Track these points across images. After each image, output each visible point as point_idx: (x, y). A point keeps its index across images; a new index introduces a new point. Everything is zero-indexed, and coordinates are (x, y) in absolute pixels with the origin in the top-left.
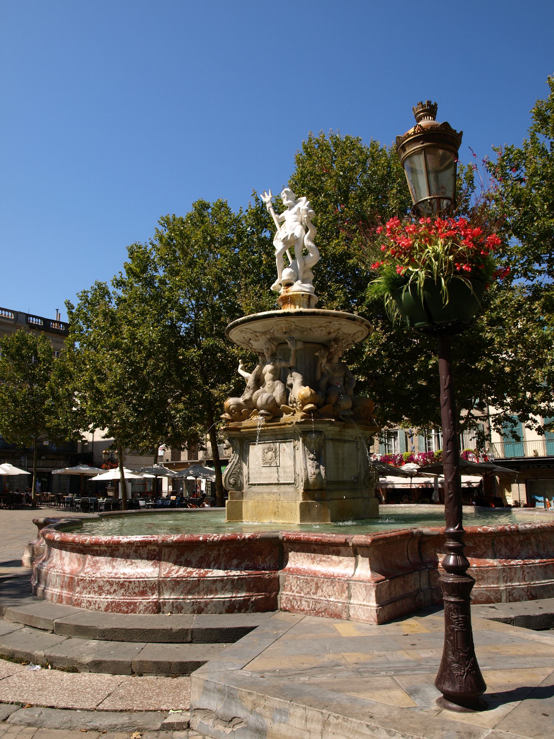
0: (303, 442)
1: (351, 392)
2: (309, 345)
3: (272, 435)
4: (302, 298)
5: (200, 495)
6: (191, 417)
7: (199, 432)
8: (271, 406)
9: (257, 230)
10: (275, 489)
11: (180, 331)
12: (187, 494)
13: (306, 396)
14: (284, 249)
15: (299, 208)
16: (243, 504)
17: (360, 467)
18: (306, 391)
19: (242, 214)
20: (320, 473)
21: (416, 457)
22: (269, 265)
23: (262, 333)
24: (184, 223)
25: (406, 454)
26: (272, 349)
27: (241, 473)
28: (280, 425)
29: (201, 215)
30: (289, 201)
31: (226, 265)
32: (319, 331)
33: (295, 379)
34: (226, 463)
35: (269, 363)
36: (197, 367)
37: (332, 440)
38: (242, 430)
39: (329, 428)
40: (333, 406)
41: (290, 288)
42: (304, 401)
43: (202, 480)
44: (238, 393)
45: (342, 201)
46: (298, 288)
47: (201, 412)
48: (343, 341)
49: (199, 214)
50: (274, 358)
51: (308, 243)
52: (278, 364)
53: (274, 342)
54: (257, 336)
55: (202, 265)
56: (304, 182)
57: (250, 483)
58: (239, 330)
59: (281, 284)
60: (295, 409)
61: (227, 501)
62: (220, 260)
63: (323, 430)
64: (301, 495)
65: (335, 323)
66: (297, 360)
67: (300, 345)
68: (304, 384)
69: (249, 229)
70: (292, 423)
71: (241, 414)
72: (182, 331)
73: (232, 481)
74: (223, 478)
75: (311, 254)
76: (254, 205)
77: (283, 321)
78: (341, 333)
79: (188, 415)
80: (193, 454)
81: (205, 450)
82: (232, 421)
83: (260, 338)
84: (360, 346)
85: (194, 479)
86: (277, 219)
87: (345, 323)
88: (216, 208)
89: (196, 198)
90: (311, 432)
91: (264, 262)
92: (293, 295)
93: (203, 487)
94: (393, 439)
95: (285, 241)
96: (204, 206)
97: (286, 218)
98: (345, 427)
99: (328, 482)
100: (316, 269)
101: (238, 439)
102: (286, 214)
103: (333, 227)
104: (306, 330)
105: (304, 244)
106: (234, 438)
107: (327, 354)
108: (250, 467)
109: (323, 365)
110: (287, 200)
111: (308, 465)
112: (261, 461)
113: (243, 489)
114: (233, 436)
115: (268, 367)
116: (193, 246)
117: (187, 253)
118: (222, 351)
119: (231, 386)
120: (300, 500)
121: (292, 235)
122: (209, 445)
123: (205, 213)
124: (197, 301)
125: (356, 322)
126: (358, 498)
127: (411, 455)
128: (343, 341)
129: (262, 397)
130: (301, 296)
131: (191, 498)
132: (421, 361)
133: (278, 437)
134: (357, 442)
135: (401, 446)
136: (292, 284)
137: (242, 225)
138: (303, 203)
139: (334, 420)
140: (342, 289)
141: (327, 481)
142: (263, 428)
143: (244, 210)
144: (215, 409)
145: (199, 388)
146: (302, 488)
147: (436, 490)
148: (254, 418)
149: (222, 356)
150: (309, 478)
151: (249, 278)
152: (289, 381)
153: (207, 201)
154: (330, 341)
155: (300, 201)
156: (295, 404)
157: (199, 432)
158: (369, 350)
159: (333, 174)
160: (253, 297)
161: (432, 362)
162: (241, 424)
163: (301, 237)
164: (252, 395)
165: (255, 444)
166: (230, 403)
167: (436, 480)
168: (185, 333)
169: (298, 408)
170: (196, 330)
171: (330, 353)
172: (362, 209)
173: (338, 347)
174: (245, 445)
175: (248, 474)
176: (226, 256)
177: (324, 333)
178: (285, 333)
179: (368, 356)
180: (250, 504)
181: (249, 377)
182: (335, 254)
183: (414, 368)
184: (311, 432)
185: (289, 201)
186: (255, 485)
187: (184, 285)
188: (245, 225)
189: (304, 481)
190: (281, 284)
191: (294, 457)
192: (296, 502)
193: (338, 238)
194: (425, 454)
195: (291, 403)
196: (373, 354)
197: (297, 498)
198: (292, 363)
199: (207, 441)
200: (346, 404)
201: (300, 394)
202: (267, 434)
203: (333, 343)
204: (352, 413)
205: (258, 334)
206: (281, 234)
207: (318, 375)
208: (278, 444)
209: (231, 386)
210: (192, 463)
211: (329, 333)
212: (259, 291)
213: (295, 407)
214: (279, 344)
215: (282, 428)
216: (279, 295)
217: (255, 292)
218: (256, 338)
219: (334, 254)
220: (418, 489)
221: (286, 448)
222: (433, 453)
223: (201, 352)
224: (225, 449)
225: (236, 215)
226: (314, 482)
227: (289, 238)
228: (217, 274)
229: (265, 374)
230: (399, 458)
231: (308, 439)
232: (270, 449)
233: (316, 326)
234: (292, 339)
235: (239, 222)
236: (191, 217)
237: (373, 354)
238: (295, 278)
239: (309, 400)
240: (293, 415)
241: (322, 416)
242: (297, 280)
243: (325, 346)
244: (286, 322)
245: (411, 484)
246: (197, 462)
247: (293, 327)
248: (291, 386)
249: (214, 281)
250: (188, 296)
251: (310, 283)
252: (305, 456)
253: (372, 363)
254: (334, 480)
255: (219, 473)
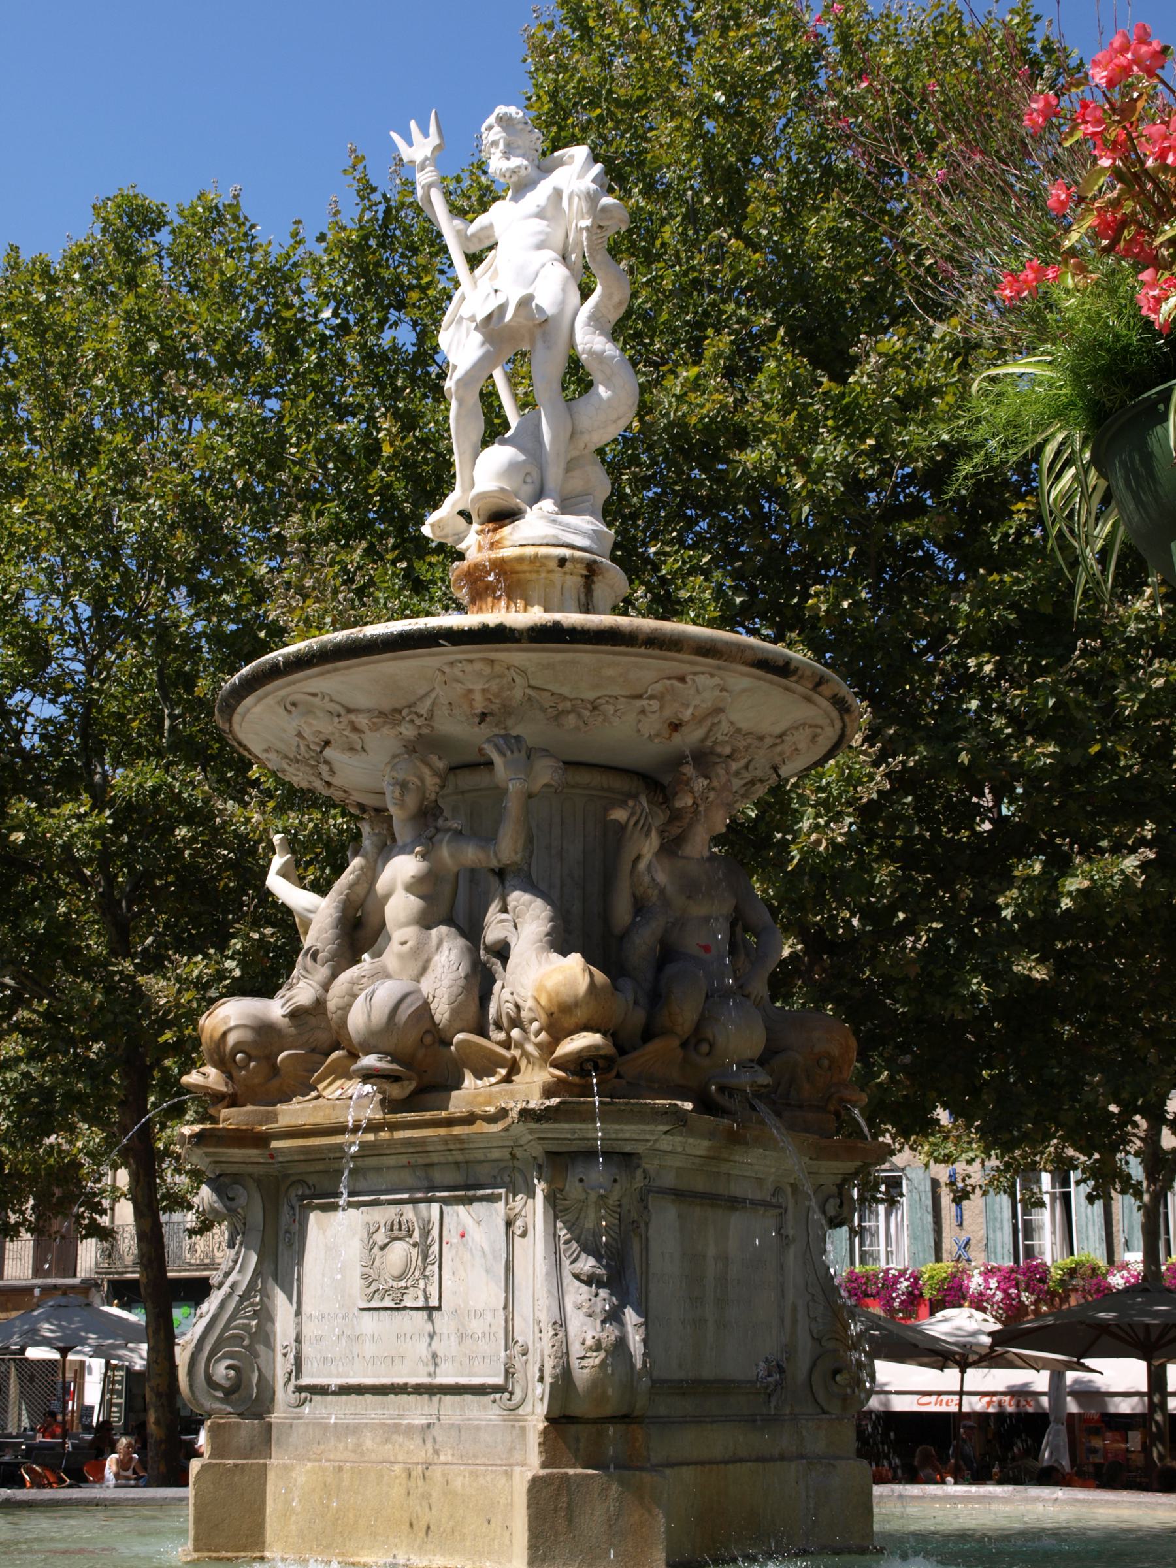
0: (550, 1199)
1: (760, 988)
2: (584, 777)
3: (409, 1166)
4: (557, 576)
5: (76, 1428)
6: (51, 1090)
7: (85, 1160)
8: (413, 1036)
9: (362, 319)
10: (417, 1411)
11: (22, 731)
12: (25, 1423)
13: (566, 995)
14: (484, 364)
15: (558, 193)
16: (271, 1476)
17: (795, 1322)
18: (570, 973)
19: (301, 250)
20: (621, 1343)
21: (975, 1283)
22: (405, 463)
23: (382, 714)
24: (54, 280)
25: (933, 1271)
26: (422, 789)
27: (263, 1335)
28: (450, 1122)
29: (126, 252)
30: (516, 162)
31: (227, 459)
32: (629, 715)
33: (522, 921)
34: (196, 1290)
35: (406, 850)
36: (85, 882)
37: (678, 1195)
38: (275, 1144)
39: (666, 1143)
40: (684, 1045)
41: (507, 530)
42: (560, 1020)
43: (88, 1360)
44: (264, 978)
45: (720, 209)
46: (539, 528)
47: (95, 1072)
48: (734, 766)
49: (117, 247)
50: (428, 823)
51: (591, 341)
52: (445, 852)
53: (434, 759)
54: (355, 729)
55: (123, 453)
56: (561, 129)
57: (305, 1381)
58: (281, 702)
59: (465, 515)
60: (516, 1053)
61: (195, 1465)
62: (200, 443)
63: (640, 1149)
64: (533, 1440)
65: (702, 680)
66: (530, 840)
67: (545, 773)
68: (560, 943)
69: (327, 314)
70: (503, 1113)
71: (275, 1070)
72: (28, 728)
73: (221, 1371)
74: (182, 1357)
75: (602, 390)
76: (352, 213)
77: (478, 666)
78: (725, 727)
79: (40, 1086)
80: (55, 1253)
81: (106, 1235)
82: (233, 1101)
83: (372, 739)
84: (779, 806)
85: (56, 1356)
86: (462, 236)
87: (746, 682)
88: (191, 229)
89: (111, 182)
90: (589, 1155)
91: (387, 450)
92: (520, 559)
93: (92, 1393)
94: (881, 1208)
95: (491, 325)
96: (141, 219)
97: (499, 233)
98: (735, 1139)
99: (660, 1386)
100: (618, 460)
101: (259, 1181)
102: (502, 217)
103: (677, 317)
104: (574, 710)
105: (572, 345)
106: (237, 1179)
107: (660, 818)
108: (307, 1308)
109: (642, 865)
110: (507, 154)
111: (569, 1307)
112: (359, 1283)
113: (270, 1411)
114: (234, 1169)
115: (403, 868)
116: (86, 378)
117: (63, 406)
118: (198, 816)
119: (229, 964)
120: (531, 1463)
121: (526, 302)
122: (125, 1212)
123: (146, 248)
124: (98, 604)
125: (789, 682)
126: (782, 1458)
127: (953, 1276)
128: (734, 766)
129: (369, 996)
130: (553, 565)
131: (39, 1438)
132: (1028, 879)
133: (438, 1176)
134: (782, 1210)
135: (914, 1237)
136: (517, 515)
137: (299, 292)
138: (576, 172)
139: (688, 1106)
140: (706, 573)
141: (653, 1382)
142: (370, 1137)
143: (309, 233)
144: (158, 1062)
145: (89, 968)
146: (542, 1409)
147: (1057, 1421)
148: (333, 1090)
149: (194, 839)
150: (575, 1364)
151: (320, 514)
152: (495, 928)
153: (153, 200)
154: (677, 761)
155: (560, 163)
156: (515, 1033)
157: (85, 1160)
158: (816, 828)
159: (685, 95)
160: (336, 591)
161: (1073, 884)
162: (273, 1117)
163: (561, 311)
164: (326, 987)
165: (334, 1207)
166: (226, 1018)
167: (1057, 1378)
168: (43, 738)
169: (530, 1048)
170: (92, 733)
171: (675, 816)
172: (798, 245)
173: (710, 788)
174: (285, 1209)
175: (298, 1340)
176: (227, 422)
177: (652, 724)
178: (483, 717)
179: (810, 852)
180: (302, 1480)
181: (316, 911)
182: (686, 425)
183: (999, 909)
184: (589, 1155)
185: (516, 162)
186: (322, 1390)
187: (43, 534)
188: (310, 295)
189: (548, 1380)
190: (465, 515)
191: (509, 1267)
192: (509, 1475)
193: (697, 359)
194: (1012, 1270)
195: (499, 1027)
196: (832, 842)
197: (517, 1456)
198: (508, 848)
199: (115, 1200)
200: (740, 1037)
201: (540, 987)
202: (390, 1161)
203: (689, 770)
204: (764, 1079)
205: (362, 721)
206: (474, 298)
207: (622, 911)
208: (435, 1207)
209: (229, 964)
210: (47, 1290)
211: (675, 727)
212: (359, 568)
213: (519, 1045)
214: (453, 769)
215: (457, 1139)
216: (461, 556)
217: (347, 572)
218: (354, 737)
219: (681, 423)
220: (982, 1417)
221: (473, 1227)
222: (1044, 1271)
223: (107, 817)
224: (192, 1232)
225: (275, 251)
226: (596, 1384)
227: (509, 316)
228: (185, 493)
229: (387, 897)
230: (904, 1285)
231: (574, 1189)
232: (398, 1232)
233: (616, 691)
234: (512, 743)
235: (287, 278)
236: (83, 259)
237: (832, 842)
238: (528, 490)
239: (581, 1015)
240: (507, 1079)
241: (634, 1088)
242: (538, 496)
243: (655, 782)
244: (487, 670)
245: (961, 1393)
246: (72, 1288)
247: (518, 693)
248: (502, 952)
249: (173, 527)
250: (59, 583)
251: (592, 514)
252: (558, 1265)
253: (828, 876)
254: (681, 1375)
255: (162, 1335)
